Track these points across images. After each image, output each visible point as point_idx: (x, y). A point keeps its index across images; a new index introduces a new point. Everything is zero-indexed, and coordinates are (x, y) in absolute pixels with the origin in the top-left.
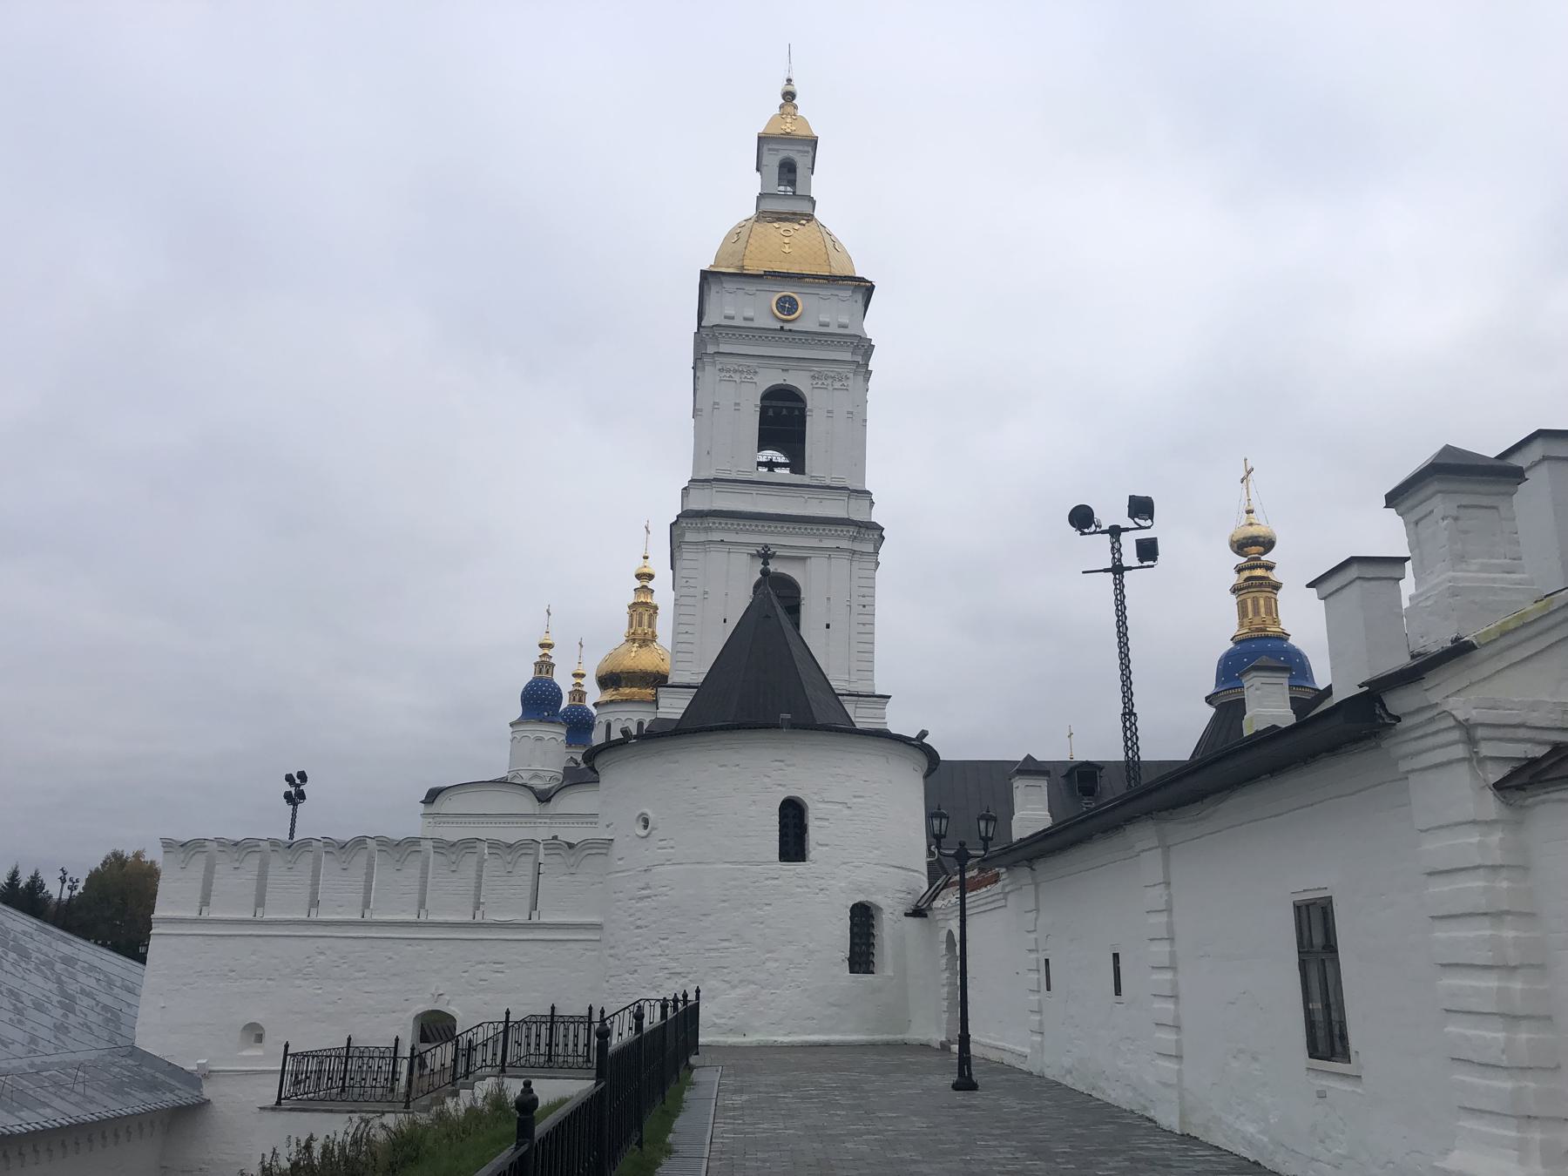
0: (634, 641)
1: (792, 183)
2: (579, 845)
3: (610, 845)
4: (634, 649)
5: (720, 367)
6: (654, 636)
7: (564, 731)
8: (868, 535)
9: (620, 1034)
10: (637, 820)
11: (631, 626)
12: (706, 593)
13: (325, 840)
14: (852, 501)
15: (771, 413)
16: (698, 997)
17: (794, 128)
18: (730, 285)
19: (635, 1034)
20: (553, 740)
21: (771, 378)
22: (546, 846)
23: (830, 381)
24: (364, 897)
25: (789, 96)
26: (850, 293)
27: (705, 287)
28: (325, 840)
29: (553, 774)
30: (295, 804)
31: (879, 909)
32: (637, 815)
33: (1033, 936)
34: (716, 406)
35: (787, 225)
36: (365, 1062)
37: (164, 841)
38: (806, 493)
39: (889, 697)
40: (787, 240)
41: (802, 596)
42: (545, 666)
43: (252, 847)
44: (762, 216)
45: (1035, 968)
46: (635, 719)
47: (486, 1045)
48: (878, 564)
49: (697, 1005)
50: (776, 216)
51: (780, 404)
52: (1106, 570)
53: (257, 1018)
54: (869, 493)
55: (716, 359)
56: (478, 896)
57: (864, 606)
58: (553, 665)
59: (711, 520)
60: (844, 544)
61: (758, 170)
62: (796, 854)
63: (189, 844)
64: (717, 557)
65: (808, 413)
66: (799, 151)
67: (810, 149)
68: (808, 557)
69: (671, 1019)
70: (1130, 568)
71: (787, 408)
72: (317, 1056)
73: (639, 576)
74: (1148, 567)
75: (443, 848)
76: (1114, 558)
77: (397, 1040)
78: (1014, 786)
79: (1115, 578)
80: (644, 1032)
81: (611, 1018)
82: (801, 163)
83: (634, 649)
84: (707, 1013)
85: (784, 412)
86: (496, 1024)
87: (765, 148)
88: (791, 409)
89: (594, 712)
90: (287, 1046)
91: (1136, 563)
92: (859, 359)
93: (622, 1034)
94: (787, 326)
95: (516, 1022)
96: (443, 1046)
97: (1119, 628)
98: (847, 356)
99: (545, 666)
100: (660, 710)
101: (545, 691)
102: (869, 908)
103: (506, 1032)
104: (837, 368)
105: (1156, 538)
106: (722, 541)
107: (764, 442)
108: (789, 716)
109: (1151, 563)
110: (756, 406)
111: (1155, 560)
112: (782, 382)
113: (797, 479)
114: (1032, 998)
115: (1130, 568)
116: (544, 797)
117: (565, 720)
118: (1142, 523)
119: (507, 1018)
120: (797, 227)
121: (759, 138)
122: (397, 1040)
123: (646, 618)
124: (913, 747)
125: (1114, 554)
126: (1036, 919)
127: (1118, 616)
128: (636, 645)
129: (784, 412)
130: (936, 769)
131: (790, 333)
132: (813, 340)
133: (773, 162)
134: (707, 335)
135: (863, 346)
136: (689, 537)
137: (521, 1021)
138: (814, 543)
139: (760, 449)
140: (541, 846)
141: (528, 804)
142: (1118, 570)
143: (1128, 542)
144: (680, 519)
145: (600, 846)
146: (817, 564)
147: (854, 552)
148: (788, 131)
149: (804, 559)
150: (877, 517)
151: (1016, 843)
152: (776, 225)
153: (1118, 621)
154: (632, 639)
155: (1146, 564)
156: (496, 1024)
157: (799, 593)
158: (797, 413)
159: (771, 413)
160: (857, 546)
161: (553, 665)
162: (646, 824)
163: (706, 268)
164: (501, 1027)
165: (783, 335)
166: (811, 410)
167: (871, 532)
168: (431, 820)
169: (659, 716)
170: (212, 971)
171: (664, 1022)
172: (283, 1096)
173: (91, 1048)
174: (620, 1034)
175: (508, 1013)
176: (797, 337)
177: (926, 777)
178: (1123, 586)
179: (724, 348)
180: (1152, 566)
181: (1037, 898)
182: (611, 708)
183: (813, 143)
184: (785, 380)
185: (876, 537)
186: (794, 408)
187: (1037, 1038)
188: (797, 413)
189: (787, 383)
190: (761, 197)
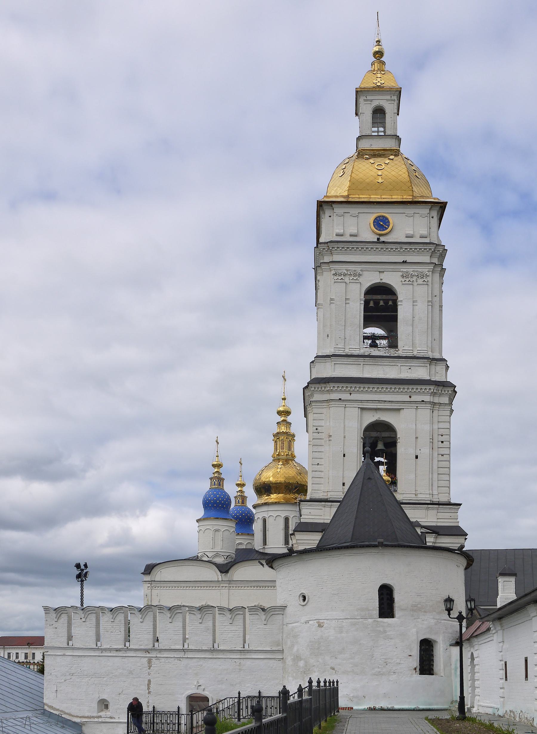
0: (279, 460)
1: (383, 124)
2: (268, 609)
3: (285, 609)
4: (280, 466)
5: (333, 272)
6: (293, 457)
7: (234, 525)
8: (445, 391)
10: (299, 596)
11: (276, 449)
12: (330, 436)
13: (130, 607)
14: (433, 367)
15: (372, 304)
16: (337, 685)
17: (383, 82)
18: (339, 210)
20: (228, 531)
23: (414, 278)
24: (213, 637)
25: (379, 54)
26: (427, 211)
27: (321, 212)
28: (130, 607)
29: (229, 554)
30: (82, 581)
31: (435, 641)
32: (299, 594)
33: (501, 654)
34: (332, 302)
35: (379, 160)
36: (168, 716)
37: (44, 607)
38: (400, 362)
39: (460, 505)
40: (380, 173)
41: (398, 436)
42: (218, 480)
43: (91, 610)
44: (361, 154)
45: (501, 669)
46: (283, 516)
47: (224, 711)
48: (452, 411)
50: (372, 153)
51: (379, 297)
53: (105, 697)
54: (444, 360)
55: (331, 266)
56: (184, 634)
57: (442, 442)
58: (223, 479)
59: (332, 385)
60: (427, 398)
61: (357, 114)
63: (58, 609)
64: (336, 411)
65: (399, 303)
66: (387, 100)
67: (395, 98)
68: (401, 409)
71: (383, 300)
73: (279, 413)
75: (194, 611)
77: (179, 708)
81: (293, 695)
82: (389, 108)
83: (280, 466)
84: (341, 693)
85: (382, 303)
86: (234, 699)
87: (361, 100)
89: (254, 511)
92: (435, 261)
93: (294, 699)
94: (382, 239)
95: (244, 698)
96: (197, 714)
98: (427, 259)
99: (218, 480)
100: (303, 517)
101: (219, 497)
102: (431, 641)
103: (239, 702)
104: (419, 268)
106: (340, 399)
107: (368, 321)
110: (371, 113)
112: (378, 281)
113: (392, 352)
114: (501, 682)
116: (224, 569)
117: (233, 517)
120: (387, 161)
121: (357, 92)
122: (179, 708)
123: (286, 444)
124: (456, 554)
126: (502, 646)
128: (281, 463)
129: (382, 303)
132: (401, 248)
133: (367, 110)
134: (324, 249)
135: (439, 251)
136: (317, 397)
137: (246, 697)
139: (365, 326)
140: (247, 610)
141: (213, 574)
144: (310, 385)
145: (278, 610)
146: (408, 413)
147: (434, 404)
148: (379, 84)
149: (399, 410)
150: (450, 378)
152: (372, 161)
154: (277, 459)
156: (234, 699)
157: (396, 435)
158: (390, 303)
159: (372, 304)
160: (436, 400)
161: (223, 479)
162: (304, 599)
163: (321, 199)
164: (236, 700)
165: (379, 246)
166: (401, 301)
167: (447, 389)
168: (149, 585)
169: (302, 521)
170: (78, 673)
172: (129, 732)
173: (25, 710)
175: (239, 693)
176: (390, 246)
177: (466, 569)
179: (336, 258)
181: (503, 636)
182: (265, 508)
183: (398, 93)
184: (381, 279)
185: (450, 392)
186: (389, 300)
187: (502, 700)
188: (390, 303)
189: (383, 281)
190: (359, 139)
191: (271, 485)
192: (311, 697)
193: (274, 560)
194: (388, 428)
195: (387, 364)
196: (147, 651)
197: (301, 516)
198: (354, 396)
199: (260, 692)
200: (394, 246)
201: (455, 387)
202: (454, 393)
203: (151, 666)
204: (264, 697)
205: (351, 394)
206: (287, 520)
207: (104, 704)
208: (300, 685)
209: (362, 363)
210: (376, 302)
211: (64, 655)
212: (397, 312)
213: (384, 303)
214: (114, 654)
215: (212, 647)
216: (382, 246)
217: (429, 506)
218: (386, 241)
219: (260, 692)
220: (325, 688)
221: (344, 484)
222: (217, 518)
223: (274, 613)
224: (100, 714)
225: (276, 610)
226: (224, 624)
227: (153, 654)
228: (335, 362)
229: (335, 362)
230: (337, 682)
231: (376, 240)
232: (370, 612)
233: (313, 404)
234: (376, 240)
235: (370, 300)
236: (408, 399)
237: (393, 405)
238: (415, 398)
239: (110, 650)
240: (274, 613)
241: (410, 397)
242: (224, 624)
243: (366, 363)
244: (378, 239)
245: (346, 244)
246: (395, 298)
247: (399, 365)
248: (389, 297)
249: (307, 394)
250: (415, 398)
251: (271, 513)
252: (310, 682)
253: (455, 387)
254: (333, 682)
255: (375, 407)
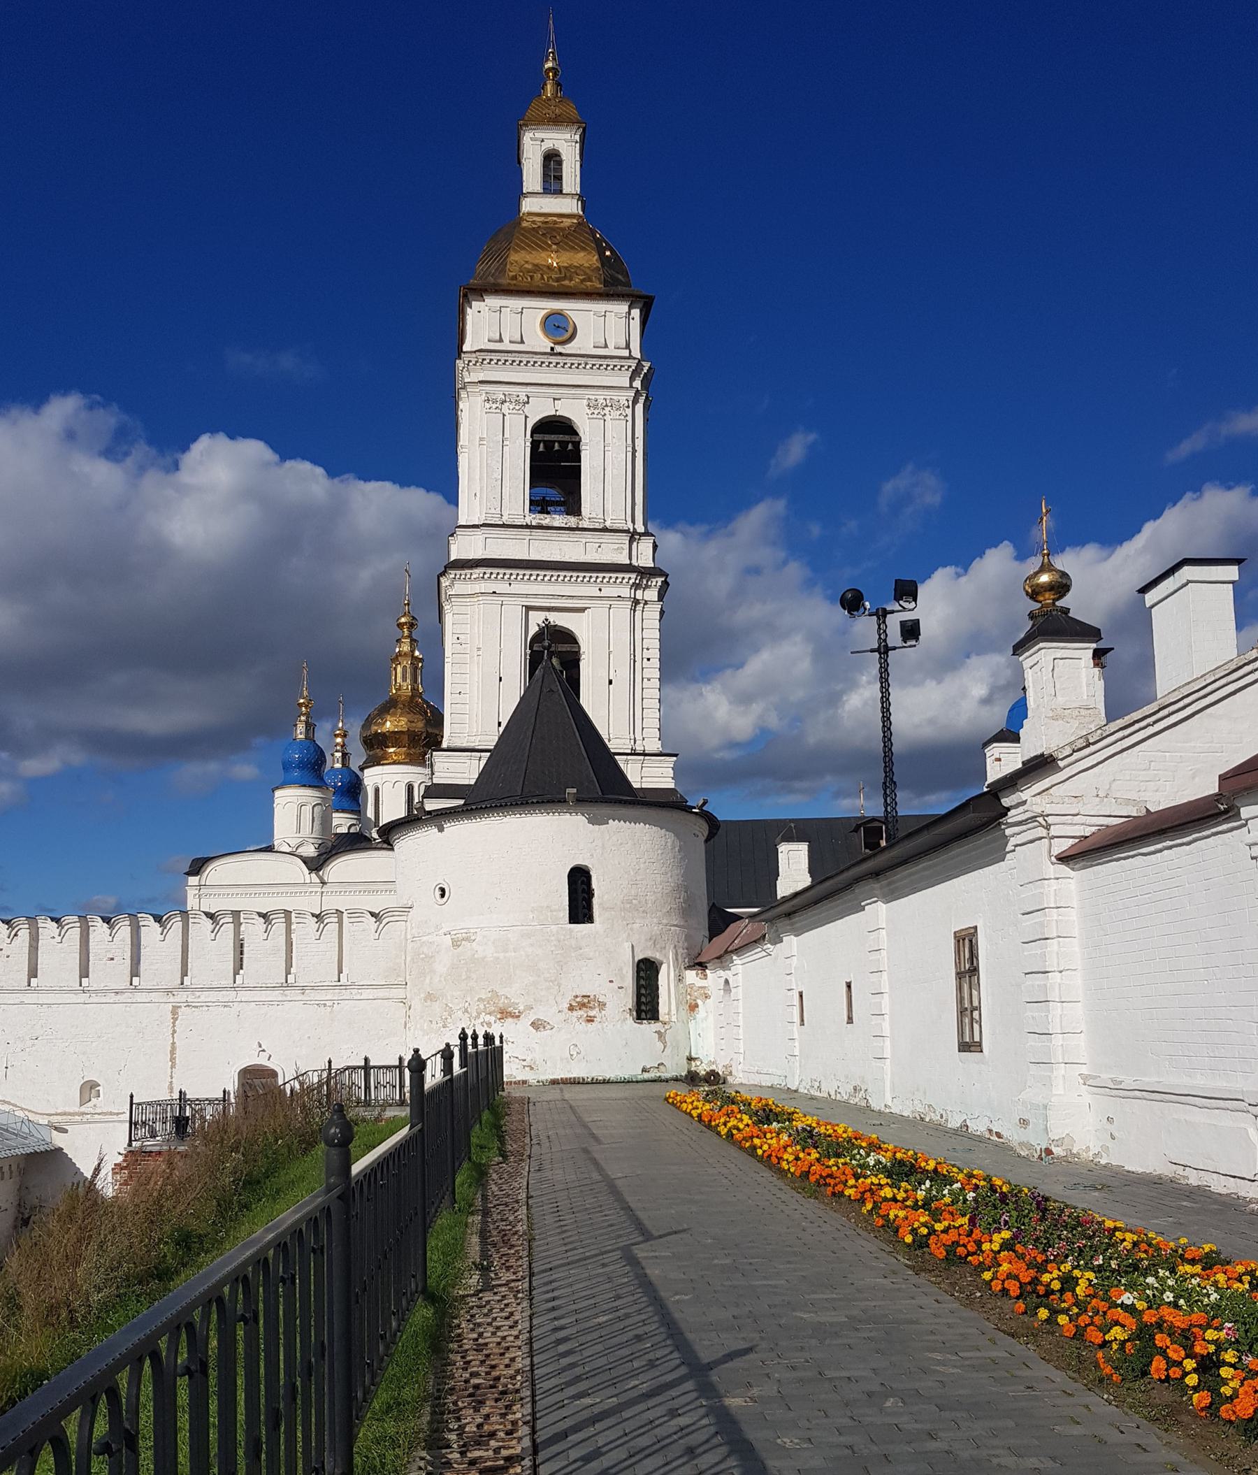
9: (433, 1076)
15: (541, 448)
16: (501, 1042)
19: (444, 1076)
21: (541, 409)
22: (349, 915)
34: (481, 442)
49: (502, 1047)
52: (872, 651)
62: (585, 915)
68: (586, 608)
69: (459, 1076)
70: (894, 648)
71: (559, 442)
72: (160, 1105)
74: (911, 646)
76: (880, 638)
78: (780, 851)
79: (880, 657)
80: (455, 1074)
85: (557, 446)
88: (563, 444)
90: (132, 1097)
91: (899, 642)
93: (433, 1076)
94: (558, 349)
97: (882, 703)
105: (918, 620)
106: (494, 593)
108: (575, 790)
109: (913, 643)
111: (917, 639)
112: (553, 413)
115: (894, 648)
118: (906, 605)
119: (330, 1066)
125: (880, 635)
127: (882, 693)
129: (557, 446)
130: (716, 834)
131: (560, 357)
138: (593, 591)
142: (884, 650)
143: (893, 622)
145: (397, 913)
146: (597, 612)
149: (582, 610)
151: (786, 900)
153: (882, 697)
155: (909, 643)
158: (570, 447)
159: (541, 448)
162: (443, 896)
165: (554, 360)
171: (448, 1077)
172: (133, 1139)
174: (433, 1076)
175: (330, 1062)
176: (569, 360)
177: (706, 841)
178: (888, 665)
180: (915, 646)
188: (570, 447)
191: (387, 734)
192: (465, 1069)
193: (389, 831)
194: (567, 637)
195: (566, 539)
196: (169, 992)
197: (433, 774)
198: (517, 588)
199: (366, 1059)
200: (576, 361)
201: (667, 576)
202: (666, 586)
203: (177, 1019)
204: (374, 1067)
205: (510, 584)
206: (410, 788)
207: (89, 1089)
208: (416, 1051)
209: (528, 538)
210: (549, 445)
211: (22, 1003)
212: (580, 462)
213: (560, 446)
214: (111, 998)
215: (284, 981)
216: (561, 360)
217: (629, 757)
218: (563, 351)
219: (366, 1059)
220: (475, 1050)
221: (499, 724)
222: (305, 786)
223: (392, 919)
224: (83, 1109)
225: (394, 913)
226: (306, 941)
227: (181, 997)
228: (487, 536)
229: (487, 536)
230: (501, 1037)
231: (549, 350)
232: (554, 913)
233: (452, 600)
234: (549, 350)
235: (540, 442)
236: (598, 594)
237: (575, 602)
238: (608, 591)
239: (105, 992)
240: (392, 919)
241: (600, 590)
242: (306, 941)
243: (534, 537)
244: (552, 349)
245: (503, 354)
246: (577, 440)
247: (584, 541)
248: (567, 438)
249: (444, 585)
250: (608, 591)
251: (386, 778)
252: (463, 1037)
253: (667, 576)
254: (475, 1037)
255: (548, 605)
